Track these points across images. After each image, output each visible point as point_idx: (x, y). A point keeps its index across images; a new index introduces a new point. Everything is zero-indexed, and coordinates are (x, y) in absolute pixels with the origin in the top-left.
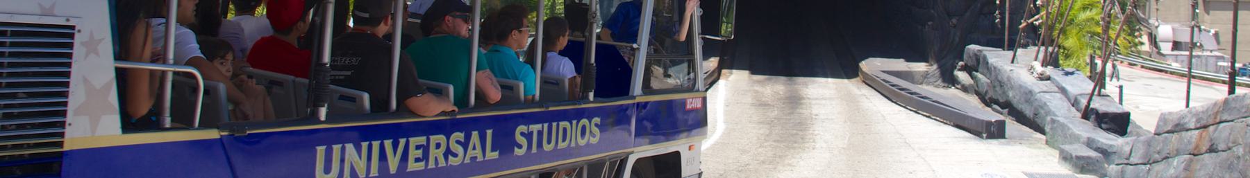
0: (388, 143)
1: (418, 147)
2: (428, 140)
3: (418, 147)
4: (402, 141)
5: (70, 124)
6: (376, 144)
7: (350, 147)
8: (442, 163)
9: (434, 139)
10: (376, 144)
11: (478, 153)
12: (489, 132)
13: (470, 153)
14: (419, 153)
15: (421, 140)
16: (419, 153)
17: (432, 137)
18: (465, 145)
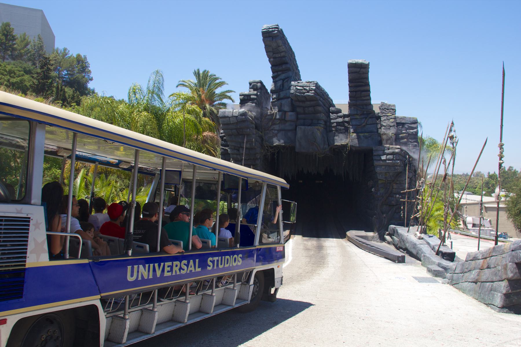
0: (156, 265)
1: (168, 266)
2: (173, 264)
3: (168, 266)
4: (162, 264)
5: (28, 257)
6: (152, 265)
7: (141, 266)
8: (178, 273)
9: (175, 263)
10: (152, 265)
11: (193, 268)
12: (197, 260)
13: (190, 269)
14: (169, 269)
15: (170, 263)
16: (169, 269)
17: (166, 263)
18: (187, 266)
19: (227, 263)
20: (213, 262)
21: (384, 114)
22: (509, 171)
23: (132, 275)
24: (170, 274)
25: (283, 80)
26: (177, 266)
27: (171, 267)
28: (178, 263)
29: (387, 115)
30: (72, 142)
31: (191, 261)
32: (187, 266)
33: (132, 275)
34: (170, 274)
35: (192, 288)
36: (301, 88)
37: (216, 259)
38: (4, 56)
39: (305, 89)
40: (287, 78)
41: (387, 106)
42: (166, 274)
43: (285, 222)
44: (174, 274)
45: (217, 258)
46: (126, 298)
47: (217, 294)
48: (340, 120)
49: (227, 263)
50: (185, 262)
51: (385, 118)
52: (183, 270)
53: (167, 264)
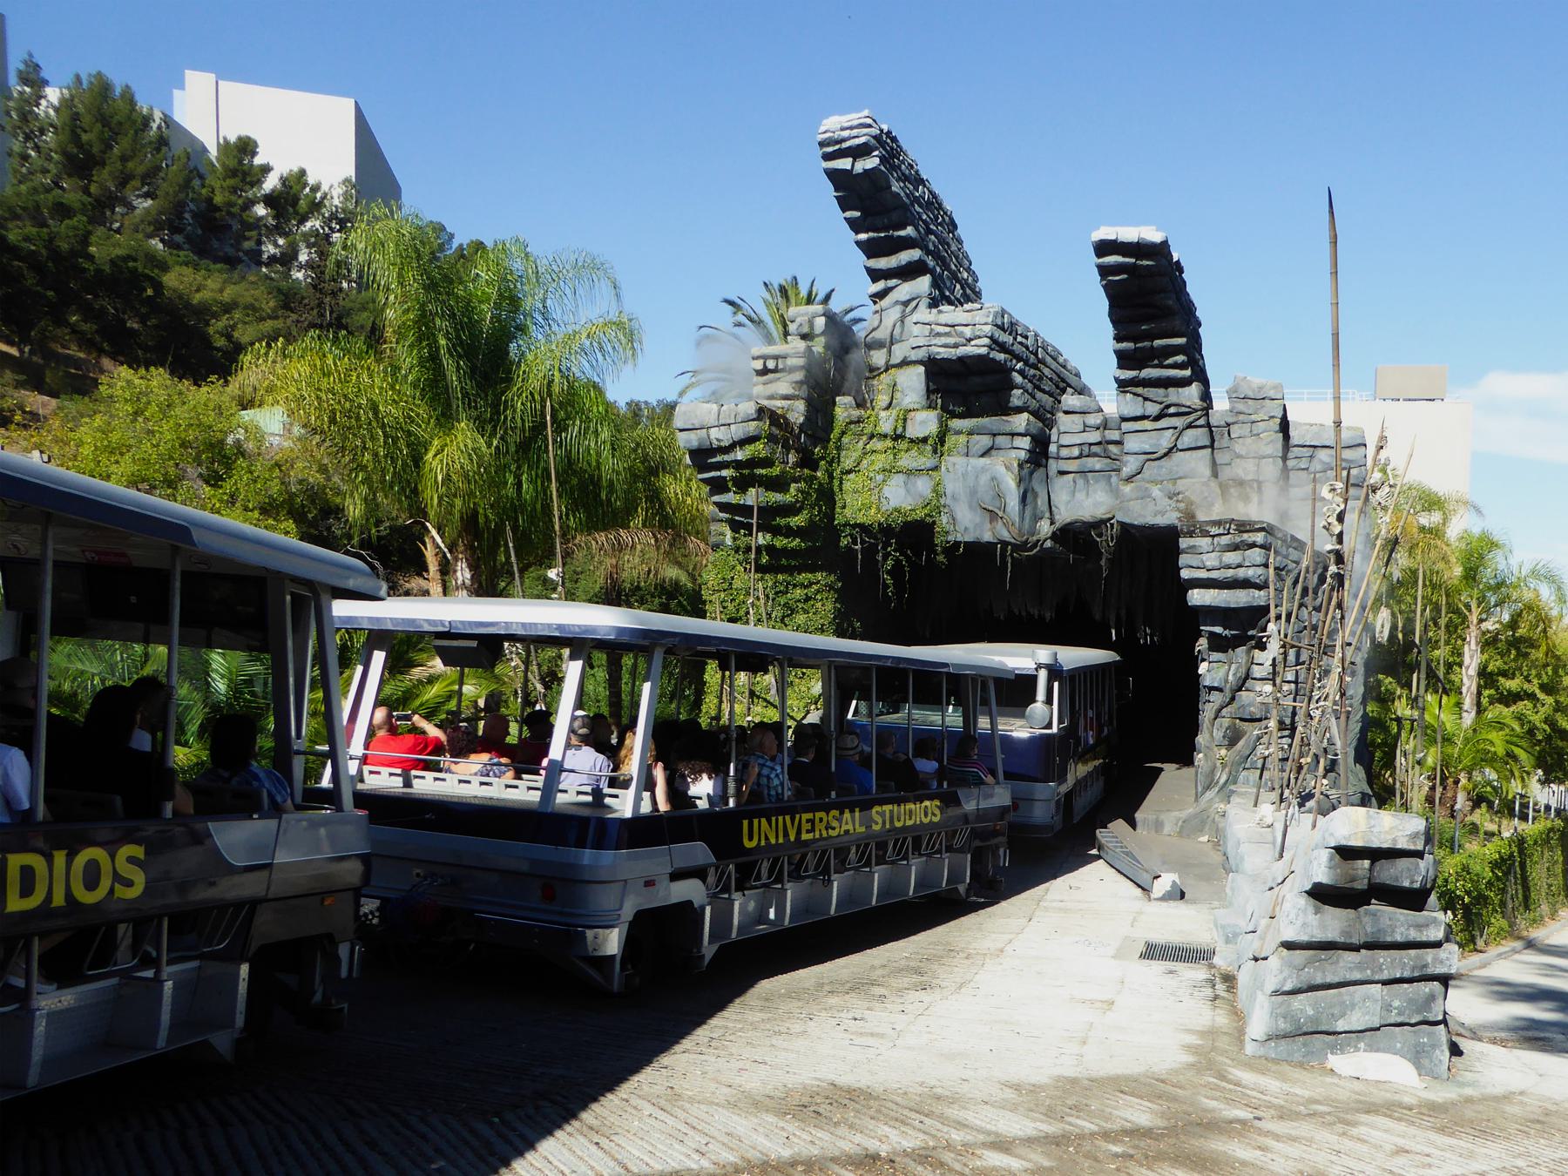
3: (808, 821)
9: (819, 815)
15: (810, 816)
16: (809, 826)
18: (840, 820)
19: (910, 819)
20: (882, 814)
21: (1241, 417)
22: (363, 919)
23: (751, 839)
24: (810, 836)
25: (906, 303)
26: (821, 820)
27: (812, 821)
28: (822, 814)
29: (1253, 417)
30: (1399, 846)
31: (792, 838)
32: (840, 820)
33: (751, 839)
34: (810, 836)
35: (1359, 445)
36: (947, 329)
37: (887, 808)
38: (246, 308)
39: (961, 335)
40: (913, 299)
41: (1253, 391)
42: (805, 836)
43: (737, 518)
44: (817, 836)
45: (890, 807)
46: (783, 861)
47: (914, 869)
48: (1094, 437)
49: (910, 819)
50: (835, 813)
51: (1246, 429)
52: (834, 829)
53: (805, 816)
